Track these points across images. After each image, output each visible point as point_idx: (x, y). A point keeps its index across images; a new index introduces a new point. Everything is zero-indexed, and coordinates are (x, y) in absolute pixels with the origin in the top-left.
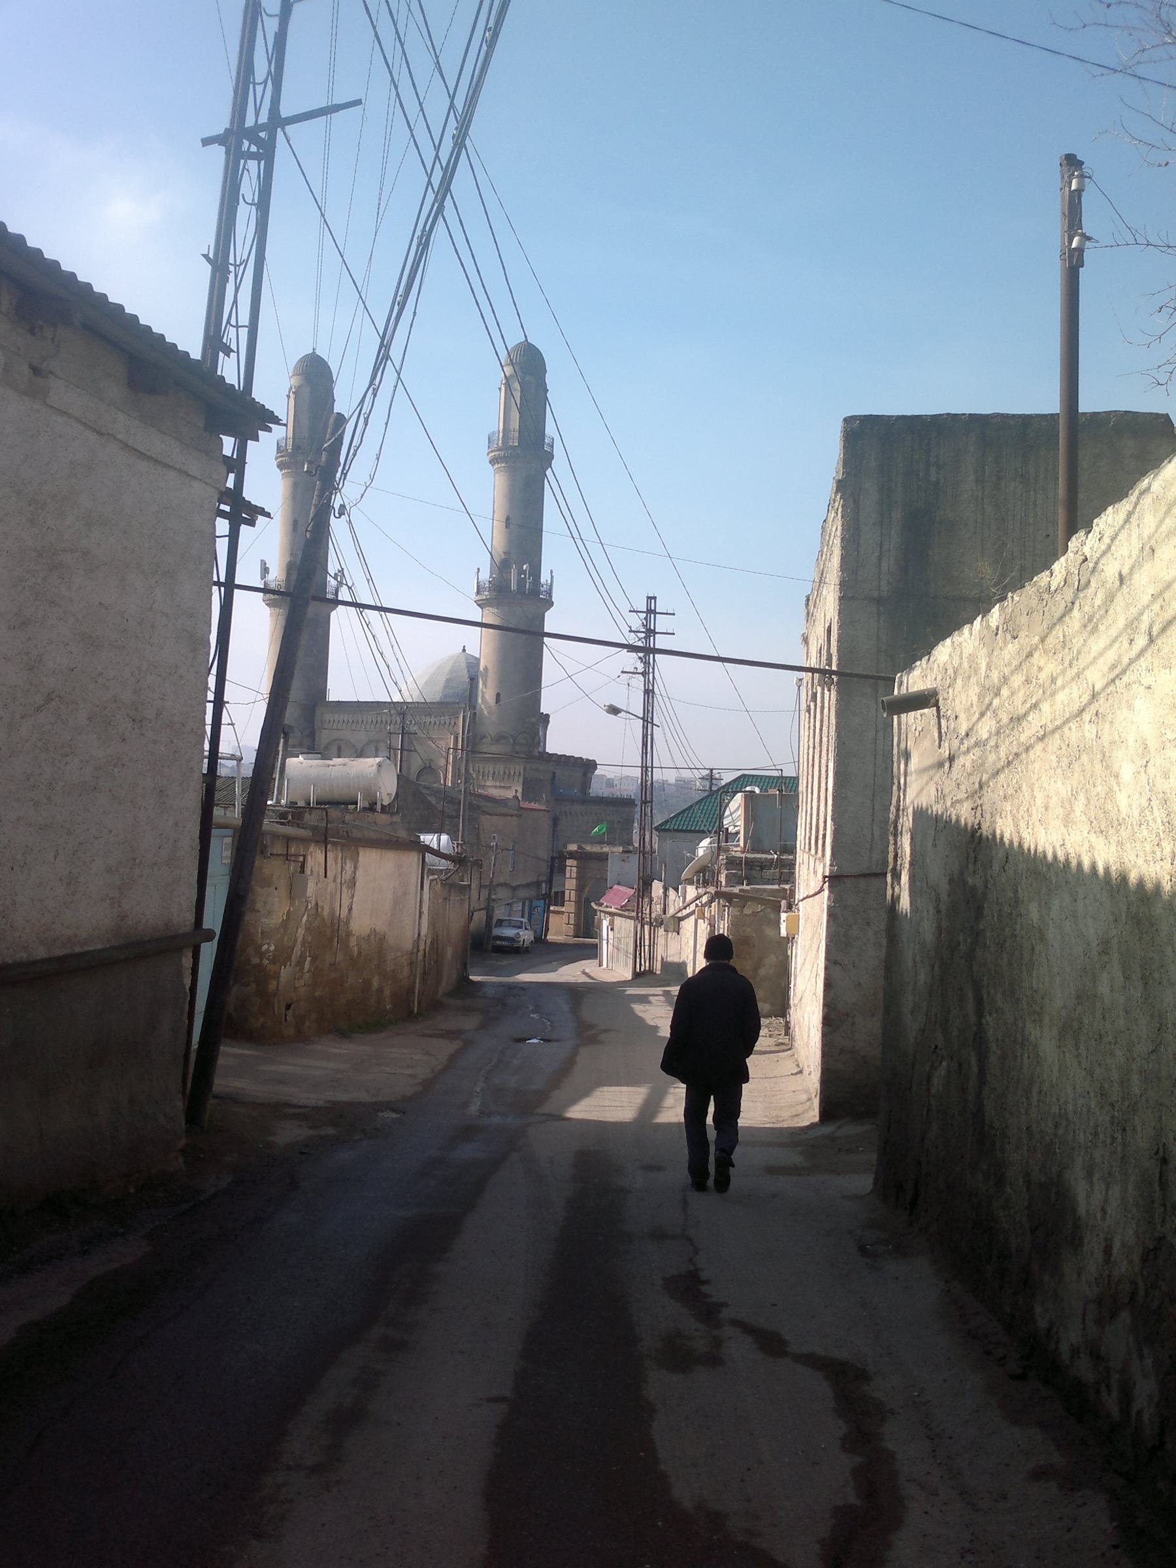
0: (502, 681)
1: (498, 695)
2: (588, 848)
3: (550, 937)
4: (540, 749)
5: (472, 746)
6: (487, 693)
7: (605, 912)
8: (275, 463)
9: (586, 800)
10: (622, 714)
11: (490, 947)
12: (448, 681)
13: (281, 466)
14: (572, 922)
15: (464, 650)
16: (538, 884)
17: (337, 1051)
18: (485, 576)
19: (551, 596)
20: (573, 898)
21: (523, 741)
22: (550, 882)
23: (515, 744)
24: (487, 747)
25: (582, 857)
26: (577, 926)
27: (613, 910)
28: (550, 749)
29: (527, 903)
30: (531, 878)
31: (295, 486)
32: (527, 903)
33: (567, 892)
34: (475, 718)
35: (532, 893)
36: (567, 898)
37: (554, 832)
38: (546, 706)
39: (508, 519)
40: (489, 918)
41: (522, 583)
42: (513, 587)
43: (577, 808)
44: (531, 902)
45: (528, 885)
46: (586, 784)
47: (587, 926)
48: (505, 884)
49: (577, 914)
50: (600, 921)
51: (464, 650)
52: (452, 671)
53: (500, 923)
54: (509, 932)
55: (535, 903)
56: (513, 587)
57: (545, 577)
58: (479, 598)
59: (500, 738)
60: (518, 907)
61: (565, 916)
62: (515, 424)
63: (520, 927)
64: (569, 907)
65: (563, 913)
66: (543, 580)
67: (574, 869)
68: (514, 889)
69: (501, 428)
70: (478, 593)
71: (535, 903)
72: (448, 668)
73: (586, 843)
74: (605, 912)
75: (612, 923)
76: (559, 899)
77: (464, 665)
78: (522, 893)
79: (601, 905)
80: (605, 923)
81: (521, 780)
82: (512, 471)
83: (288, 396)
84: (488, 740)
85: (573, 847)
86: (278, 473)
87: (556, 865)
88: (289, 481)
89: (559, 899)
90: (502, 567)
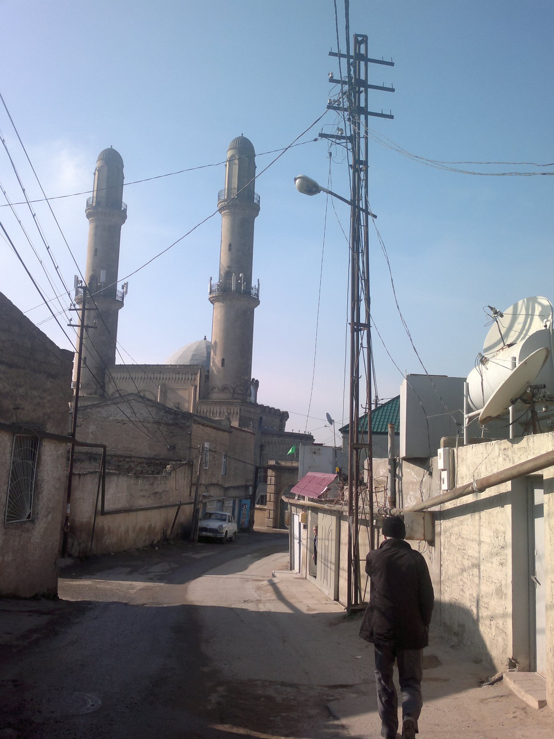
0: (226, 350)
1: (223, 360)
2: (283, 464)
3: (256, 527)
4: (247, 378)
5: (205, 394)
6: (216, 359)
7: (297, 506)
8: (85, 214)
9: (281, 433)
10: (322, 195)
11: (197, 538)
12: (194, 355)
13: (88, 216)
14: (272, 516)
15: (205, 339)
16: (246, 487)
17: (315, 504)
18: (216, 281)
19: (258, 296)
20: (272, 499)
21: (240, 392)
22: (255, 487)
23: (234, 392)
24: (216, 396)
25: (277, 469)
26: (275, 519)
27: (306, 502)
28: (260, 401)
29: (237, 502)
30: (240, 482)
31: (96, 227)
32: (237, 502)
33: (268, 495)
34: (207, 377)
35: (241, 493)
36: (268, 499)
37: (261, 454)
38: (255, 374)
39: (230, 245)
40: (196, 511)
41: (238, 285)
42: (233, 288)
43: (275, 439)
44: (240, 501)
45: (238, 487)
46: (282, 425)
47: (281, 520)
48: (217, 485)
49: (275, 511)
50: (291, 516)
51: (205, 339)
52: (197, 349)
53: (208, 516)
54: (213, 524)
55: (244, 501)
56: (233, 288)
57: (254, 283)
58: (211, 296)
59: (224, 389)
60: (229, 504)
61: (267, 513)
62: (235, 185)
63: (225, 520)
64: (270, 506)
65: (265, 510)
66: (253, 285)
67: (273, 478)
68: (226, 489)
69: (226, 187)
70: (210, 293)
71: (244, 501)
72: (194, 347)
73: (282, 460)
74: (297, 506)
75: (305, 519)
76: (263, 501)
77: (204, 346)
78: (233, 493)
79: (292, 496)
80: (297, 519)
81: (238, 416)
82: (233, 215)
83: (95, 174)
84: (216, 390)
85: (272, 463)
86: (87, 221)
87: (259, 476)
88: (93, 224)
89: (263, 501)
90: (227, 275)
